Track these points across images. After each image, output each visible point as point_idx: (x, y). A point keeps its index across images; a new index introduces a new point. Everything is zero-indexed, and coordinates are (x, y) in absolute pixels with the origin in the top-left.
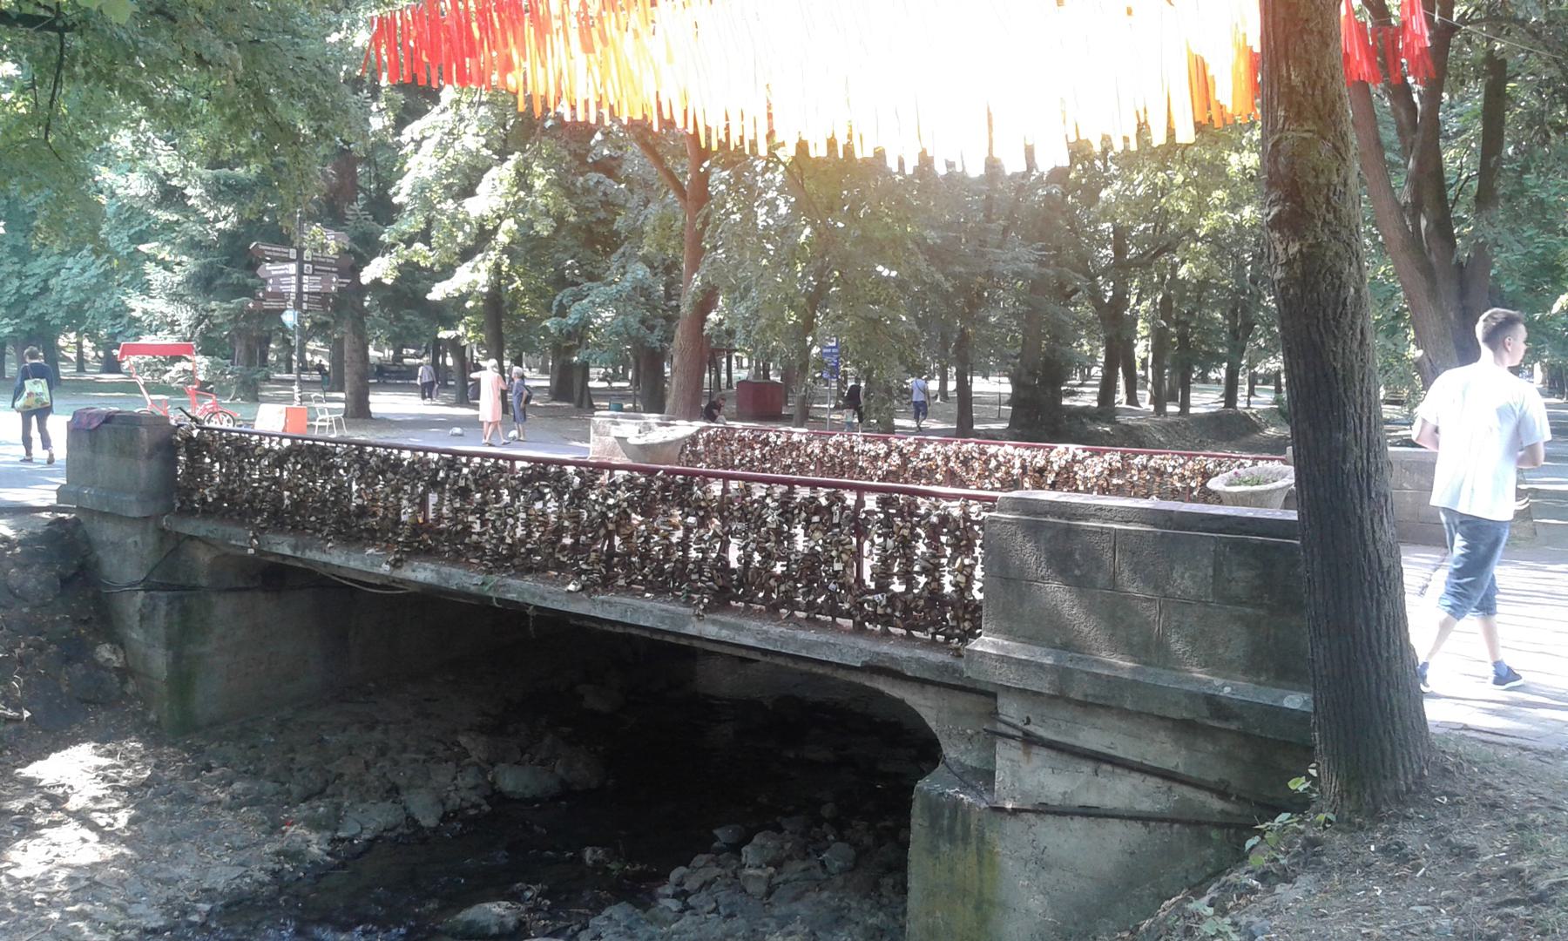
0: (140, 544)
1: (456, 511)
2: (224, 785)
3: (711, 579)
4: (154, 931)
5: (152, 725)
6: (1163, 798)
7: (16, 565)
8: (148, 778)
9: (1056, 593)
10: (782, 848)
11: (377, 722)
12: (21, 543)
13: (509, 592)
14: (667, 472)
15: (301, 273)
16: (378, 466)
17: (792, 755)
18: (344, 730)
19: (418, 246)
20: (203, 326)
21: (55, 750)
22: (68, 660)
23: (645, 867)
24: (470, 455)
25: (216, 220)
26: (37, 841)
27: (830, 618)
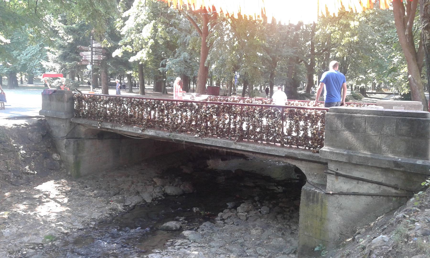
0: (65, 126)
1: (159, 116)
2: (92, 192)
3: (238, 133)
4: (81, 229)
5: (69, 176)
6: (378, 190)
7: (30, 132)
8: (70, 190)
9: (347, 134)
10: (249, 207)
11: (129, 175)
12: (31, 126)
13: (177, 137)
14: (224, 104)
15: (92, 54)
16: (136, 104)
17: (243, 184)
18: (121, 177)
19: (128, 46)
20: (63, 70)
21: (45, 182)
22: (45, 158)
23: (211, 213)
24: (164, 100)
25: (67, 40)
26: (44, 206)
27: (274, 143)
